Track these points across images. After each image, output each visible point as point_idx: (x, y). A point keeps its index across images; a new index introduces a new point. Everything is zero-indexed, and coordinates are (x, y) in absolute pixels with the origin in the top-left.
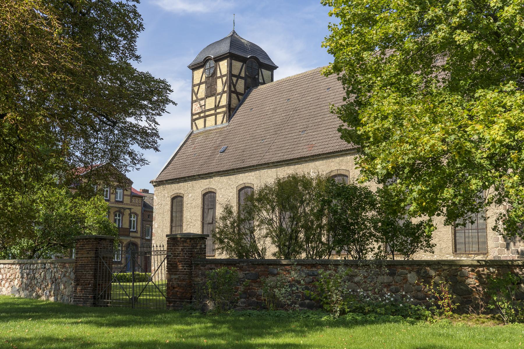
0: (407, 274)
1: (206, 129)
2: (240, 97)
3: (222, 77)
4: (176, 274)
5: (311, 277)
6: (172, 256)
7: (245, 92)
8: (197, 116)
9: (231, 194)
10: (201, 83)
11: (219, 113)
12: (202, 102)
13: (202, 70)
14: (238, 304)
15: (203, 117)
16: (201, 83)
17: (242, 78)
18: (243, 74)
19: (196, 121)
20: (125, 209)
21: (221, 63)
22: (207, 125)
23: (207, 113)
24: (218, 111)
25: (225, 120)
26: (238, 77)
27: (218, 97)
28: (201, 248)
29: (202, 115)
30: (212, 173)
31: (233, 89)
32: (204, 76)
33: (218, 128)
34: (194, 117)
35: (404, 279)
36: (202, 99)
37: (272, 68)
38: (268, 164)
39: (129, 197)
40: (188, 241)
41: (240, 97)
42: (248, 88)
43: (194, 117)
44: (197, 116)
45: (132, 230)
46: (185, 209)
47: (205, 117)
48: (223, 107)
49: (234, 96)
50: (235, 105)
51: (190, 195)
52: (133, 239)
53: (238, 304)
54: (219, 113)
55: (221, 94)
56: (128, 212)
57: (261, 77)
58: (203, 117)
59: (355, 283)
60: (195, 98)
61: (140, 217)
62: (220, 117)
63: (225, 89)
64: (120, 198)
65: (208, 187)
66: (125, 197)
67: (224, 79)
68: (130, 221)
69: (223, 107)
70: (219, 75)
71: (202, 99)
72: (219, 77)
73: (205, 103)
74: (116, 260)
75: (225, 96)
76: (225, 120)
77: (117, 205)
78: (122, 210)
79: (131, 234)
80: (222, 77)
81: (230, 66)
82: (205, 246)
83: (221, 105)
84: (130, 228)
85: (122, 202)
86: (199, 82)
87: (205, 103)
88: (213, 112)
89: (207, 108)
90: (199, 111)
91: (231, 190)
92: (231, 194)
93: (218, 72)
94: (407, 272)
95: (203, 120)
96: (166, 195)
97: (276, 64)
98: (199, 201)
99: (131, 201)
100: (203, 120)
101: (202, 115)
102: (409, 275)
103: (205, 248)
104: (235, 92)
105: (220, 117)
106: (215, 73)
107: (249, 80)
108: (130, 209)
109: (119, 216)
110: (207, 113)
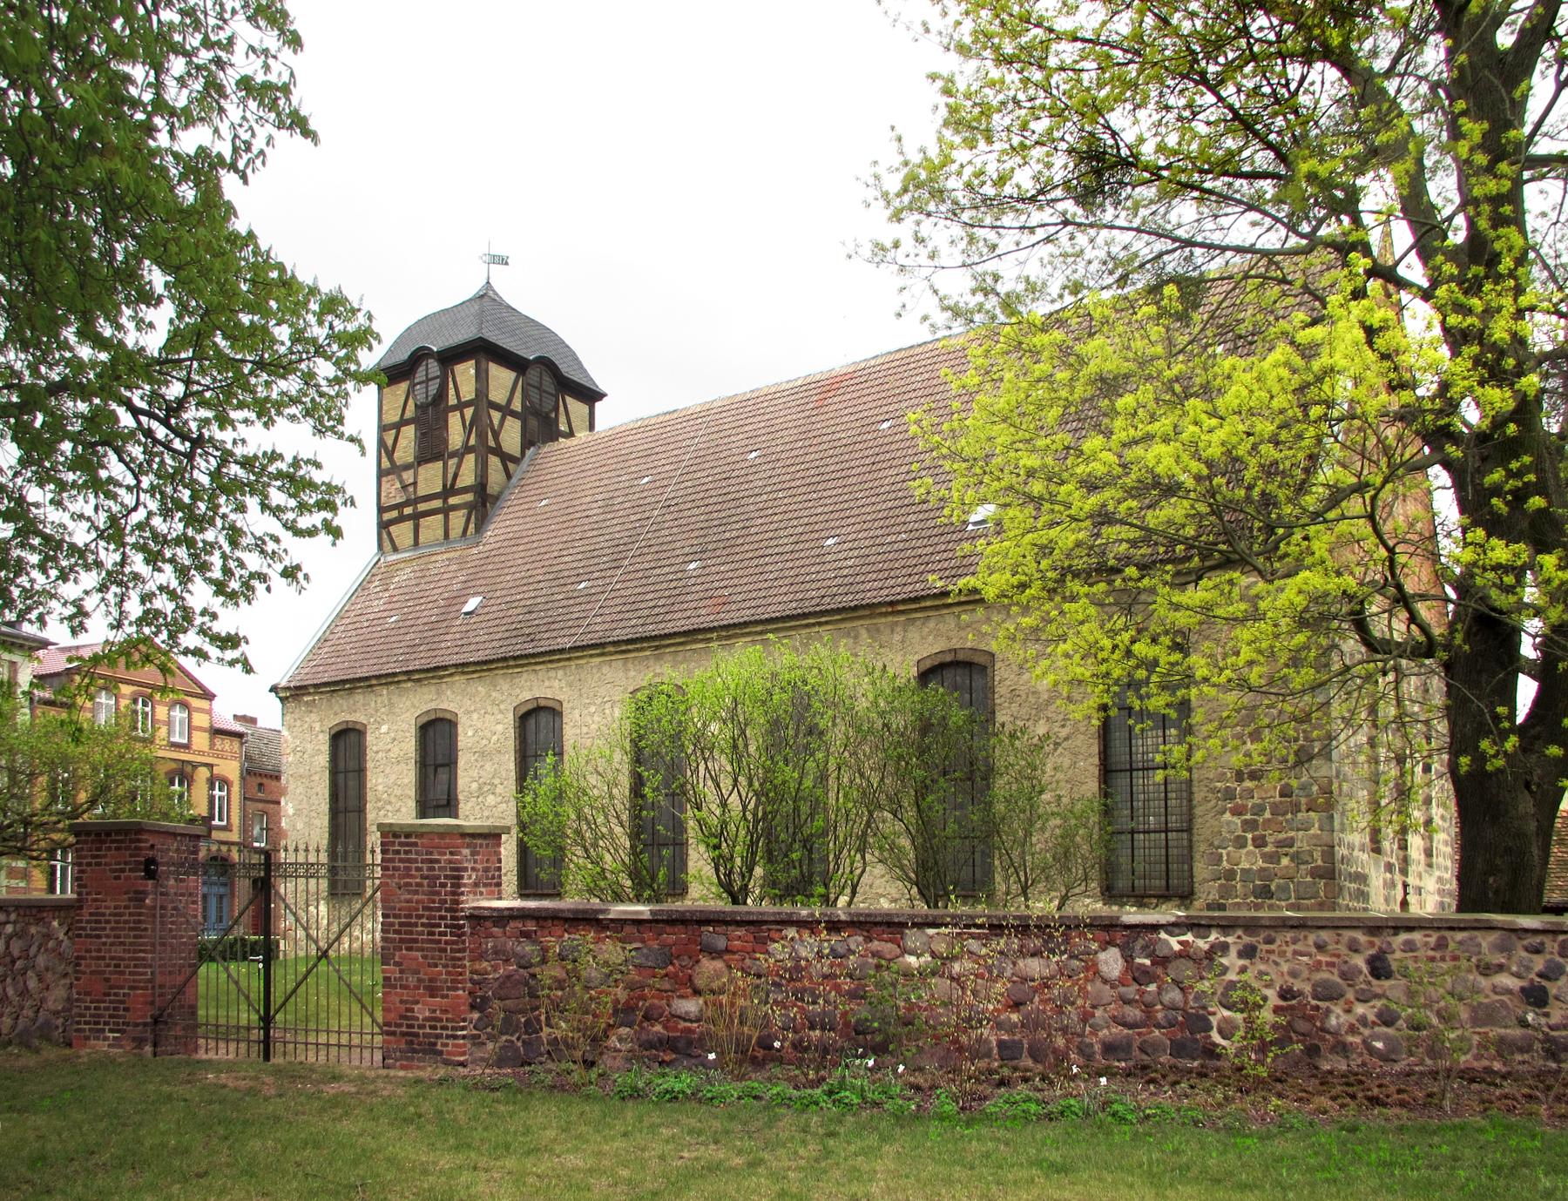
3: (461, 406)
7: (523, 454)
8: (395, 514)
9: (500, 728)
10: (403, 422)
11: (455, 508)
12: (408, 476)
13: (404, 386)
15: (409, 517)
16: (403, 422)
17: (514, 414)
18: (517, 405)
19: (392, 528)
20: (195, 765)
21: (459, 368)
23: (422, 507)
24: (453, 501)
25: (472, 526)
27: (453, 462)
29: (408, 511)
30: (445, 668)
31: (492, 443)
32: (411, 403)
34: (387, 516)
36: (407, 467)
38: (603, 645)
42: (532, 444)
43: (387, 516)
44: (395, 514)
46: (370, 765)
47: (417, 517)
48: (465, 490)
49: (494, 461)
51: (384, 728)
54: (455, 508)
55: (460, 455)
56: (203, 773)
57: (562, 419)
58: (409, 517)
60: (386, 464)
61: (236, 789)
63: (472, 442)
65: (433, 705)
66: (195, 734)
67: (469, 412)
68: (211, 799)
69: (465, 490)
70: (452, 401)
71: (407, 467)
75: (470, 459)
76: (472, 526)
78: (189, 769)
80: (461, 406)
81: (482, 377)
83: (460, 484)
85: (187, 747)
86: (397, 419)
88: (437, 503)
89: (421, 493)
90: (399, 500)
91: (500, 716)
92: (500, 728)
93: (452, 392)
95: (409, 525)
97: (602, 384)
98: (410, 746)
99: (212, 745)
100: (409, 525)
101: (408, 511)
102: (1102, 956)
104: (498, 451)
106: (442, 394)
107: (533, 423)
108: (210, 766)
110: (422, 507)
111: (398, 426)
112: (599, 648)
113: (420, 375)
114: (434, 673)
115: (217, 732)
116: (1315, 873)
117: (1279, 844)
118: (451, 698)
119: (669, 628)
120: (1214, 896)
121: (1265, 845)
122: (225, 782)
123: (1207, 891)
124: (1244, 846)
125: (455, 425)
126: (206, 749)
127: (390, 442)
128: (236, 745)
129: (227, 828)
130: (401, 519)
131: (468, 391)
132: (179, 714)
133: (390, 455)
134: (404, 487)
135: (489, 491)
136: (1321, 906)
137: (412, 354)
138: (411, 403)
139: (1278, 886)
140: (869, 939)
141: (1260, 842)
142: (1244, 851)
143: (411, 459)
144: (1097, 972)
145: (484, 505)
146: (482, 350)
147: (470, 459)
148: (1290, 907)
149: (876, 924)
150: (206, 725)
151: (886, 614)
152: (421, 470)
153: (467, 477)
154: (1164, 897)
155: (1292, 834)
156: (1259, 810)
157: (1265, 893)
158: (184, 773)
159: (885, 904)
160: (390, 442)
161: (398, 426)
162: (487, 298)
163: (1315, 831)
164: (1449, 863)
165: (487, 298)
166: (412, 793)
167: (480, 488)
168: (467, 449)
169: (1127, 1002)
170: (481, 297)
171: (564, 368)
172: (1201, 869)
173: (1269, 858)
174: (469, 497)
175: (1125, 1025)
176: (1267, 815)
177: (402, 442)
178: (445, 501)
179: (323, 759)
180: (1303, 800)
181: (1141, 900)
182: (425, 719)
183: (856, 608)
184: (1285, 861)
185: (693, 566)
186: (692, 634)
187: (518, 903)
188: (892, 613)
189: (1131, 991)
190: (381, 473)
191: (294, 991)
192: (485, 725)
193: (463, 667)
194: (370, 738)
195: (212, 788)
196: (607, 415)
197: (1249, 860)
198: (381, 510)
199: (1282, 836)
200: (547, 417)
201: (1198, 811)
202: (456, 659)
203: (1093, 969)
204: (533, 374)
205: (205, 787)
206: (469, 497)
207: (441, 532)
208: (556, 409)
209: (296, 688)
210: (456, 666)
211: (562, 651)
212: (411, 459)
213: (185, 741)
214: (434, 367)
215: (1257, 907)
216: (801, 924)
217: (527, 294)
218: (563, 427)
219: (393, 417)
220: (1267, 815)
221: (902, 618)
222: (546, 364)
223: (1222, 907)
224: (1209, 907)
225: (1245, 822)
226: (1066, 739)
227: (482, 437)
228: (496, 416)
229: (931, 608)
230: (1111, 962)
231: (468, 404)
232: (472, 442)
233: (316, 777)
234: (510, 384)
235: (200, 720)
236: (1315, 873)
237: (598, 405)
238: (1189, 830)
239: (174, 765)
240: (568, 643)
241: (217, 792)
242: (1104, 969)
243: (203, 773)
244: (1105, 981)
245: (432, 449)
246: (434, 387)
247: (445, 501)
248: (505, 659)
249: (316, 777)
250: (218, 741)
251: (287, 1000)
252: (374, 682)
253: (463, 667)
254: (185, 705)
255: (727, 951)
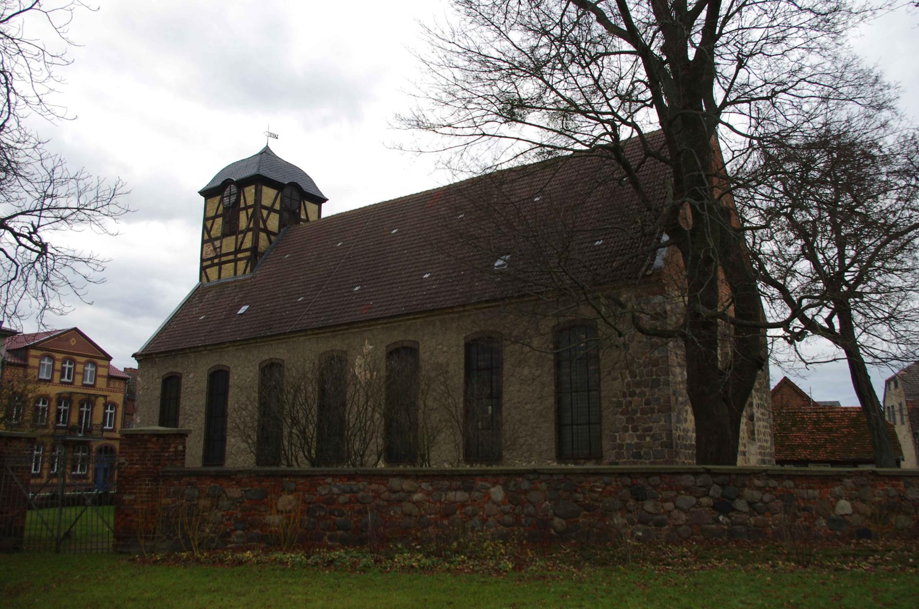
0: (489, 488)
1: (222, 281)
2: (272, 238)
3: (247, 208)
4: (131, 493)
5: (348, 495)
6: (127, 463)
7: (279, 230)
8: (209, 263)
9: (251, 374)
10: (216, 216)
11: (241, 259)
12: (217, 244)
13: (218, 198)
14: (231, 540)
15: (216, 264)
16: (216, 216)
17: (276, 211)
18: (277, 206)
19: (208, 270)
20: (97, 396)
21: (247, 189)
22: (222, 275)
23: (224, 259)
24: (239, 256)
25: (249, 268)
26: (271, 209)
27: (240, 236)
28: (176, 452)
29: (216, 261)
30: (224, 343)
31: (262, 226)
32: (221, 206)
33: (239, 281)
34: (205, 264)
35: (485, 496)
36: (217, 239)
37: (320, 200)
38: (306, 330)
39: (105, 380)
40: (154, 439)
41: (272, 238)
42: (285, 225)
43: (205, 264)
44: (209, 263)
45: (107, 427)
46: (182, 395)
47: (220, 264)
48: (246, 250)
49: (263, 235)
50: (263, 249)
51: (191, 375)
52: (108, 442)
53: (231, 540)
54: (241, 259)
55: (245, 232)
56: (101, 401)
57: (303, 212)
58: (216, 264)
59: (414, 503)
60: (206, 237)
61: (120, 409)
62: (241, 265)
63: (251, 226)
64: (91, 380)
65: (217, 363)
66: (98, 379)
67: (250, 211)
68: (105, 415)
69: (246, 250)
70: (242, 205)
71: (217, 239)
72: (243, 209)
73: (221, 243)
74: (79, 472)
75: (250, 235)
76: (249, 268)
77: (85, 391)
78: (93, 398)
79: (105, 434)
80: (247, 208)
81: (258, 194)
82: (184, 447)
83: (243, 247)
84: (104, 423)
85: (93, 386)
86: (213, 214)
87: (221, 243)
88: (231, 257)
89: (223, 252)
90: (212, 256)
91: (252, 368)
92: (251, 374)
93: (242, 201)
94: (489, 485)
95: (217, 268)
96: (156, 375)
97: (326, 195)
98: (204, 384)
99: (108, 385)
100: (217, 268)
101: (216, 261)
102: (492, 490)
103: (184, 451)
104: (265, 230)
105: (241, 265)
106: (238, 201)
107: (286, 215)
108: (105, 397)
109: (88, 407)
110: (224, 259)
111: (213, 218)
112: (304, 331)
113: (226, 193)
114: (219, 346)
115: (111, 378)
116: (662, 445)
117: (645, 430)
118: (228, 359)
119: (340, 321)
120: (613, 458)
121: (638, 430)
122: (114, 405)
123: (609, 454)
124: (627, 431)
125: (243, 217)
126: (104, 387)
127: (209, 226)
128: (122, 385)
129: (113, 431)
130: (213, 265)
131: (250, 200)
132: (90, 368)
133: (209, 233)
134: (215, 249)
135: (259, 250)
136: (666, 462)
137: (223, 182)
138: (221, 206)
139: (645, 453)
140: (370, 483)
141: (635, 429)
142: (627, 434)
143: (219, 235)
144: (490, 498)
145: (256, 258)
146: (259, 180)
147: (250, 235)
148: (652, 463)
149: (374, 475)
150: (105, 374)
151: (449, 313)
152: (225, 240)
153: (248, 244)
154: (588, 459)
155: (651, 424)
156: (635, 412)
157: (638, 456)
158: (89, 401)
159: (447, 466)
160: (209, 226)
161: (213, 218)
162: (266, 152)
163: (662, 423)
164: (769, 438)
165: (266, 152)
166: (204, 410)
167: (254, 249)
168: (248, 229)
169: (505, 513)
170: (261, 153)
171: (304, 187)
172: (606, 444)
173: (638, 437)
174: (248, 254)
175: (505, 525)
176: (639, 415)
177: (215, 227)
178: (236, 256)
179: (158, 393)
180: (656, 407)
181: (575, 459)
182: (213, 370)
183: (433, 310)
184: (648, 439)
185: (357, 288)
186: (350, 324)
187: (554, 465)
188: (452, 313)
189: (507, 508)
190: (204, 242)
191: (80, 515)
192: (244, 373)
193: (233, 343)
194: (183, 381)
195: (106, 408)
196: (327, 211)
197: (630, 439)
198: (202, 260)
199: (646, 425)
200: (294, 212)
201: (605, 413)
202: (231, 338)
203: (488, 497)
204: (287, 191)
205: (102, 408)
206: (248, 254)
207: (232, 272)
208: (300, 208)
209: (146, 355)
210: (230, 342)
211: (285, 334)
212: (219, 235)
213: (92, 383)
214: (234, 189)
215: (634, 463)
216: (334, 476)
217: (284, 152)
218: (303, 217)
219: (211, 214)
220: (639, 415)
221: (457, 315)
222: (295, 186)
223: (617, 464)
224: (610, 464)
225: (627, 419)
226: (538, 376)
227: (256, 223)
228: (265, 213)
229: (485, 308)
230: (497, 493)
231: (250, 207)
232: (251, 226)
233: (154, 403)
234: (274, 196)
235: (102, 371)
236: (662, 445)
237: (323, 205)
238: (600, 423)
239: (84, 397)
240: (288, 329)
241: (109, 411)
242: (493, 496)
243: (101, 401)
244: (494, 503)
245: (231, 229)
246: (233, 199)
247: (236, 256)
248: (255, 338)
249: (154, 403)
250: (112, 383)
251: (77, 520)
252: (310, 332)
253: (233, 343)
254: (95, 364)
255: (296, 490)
